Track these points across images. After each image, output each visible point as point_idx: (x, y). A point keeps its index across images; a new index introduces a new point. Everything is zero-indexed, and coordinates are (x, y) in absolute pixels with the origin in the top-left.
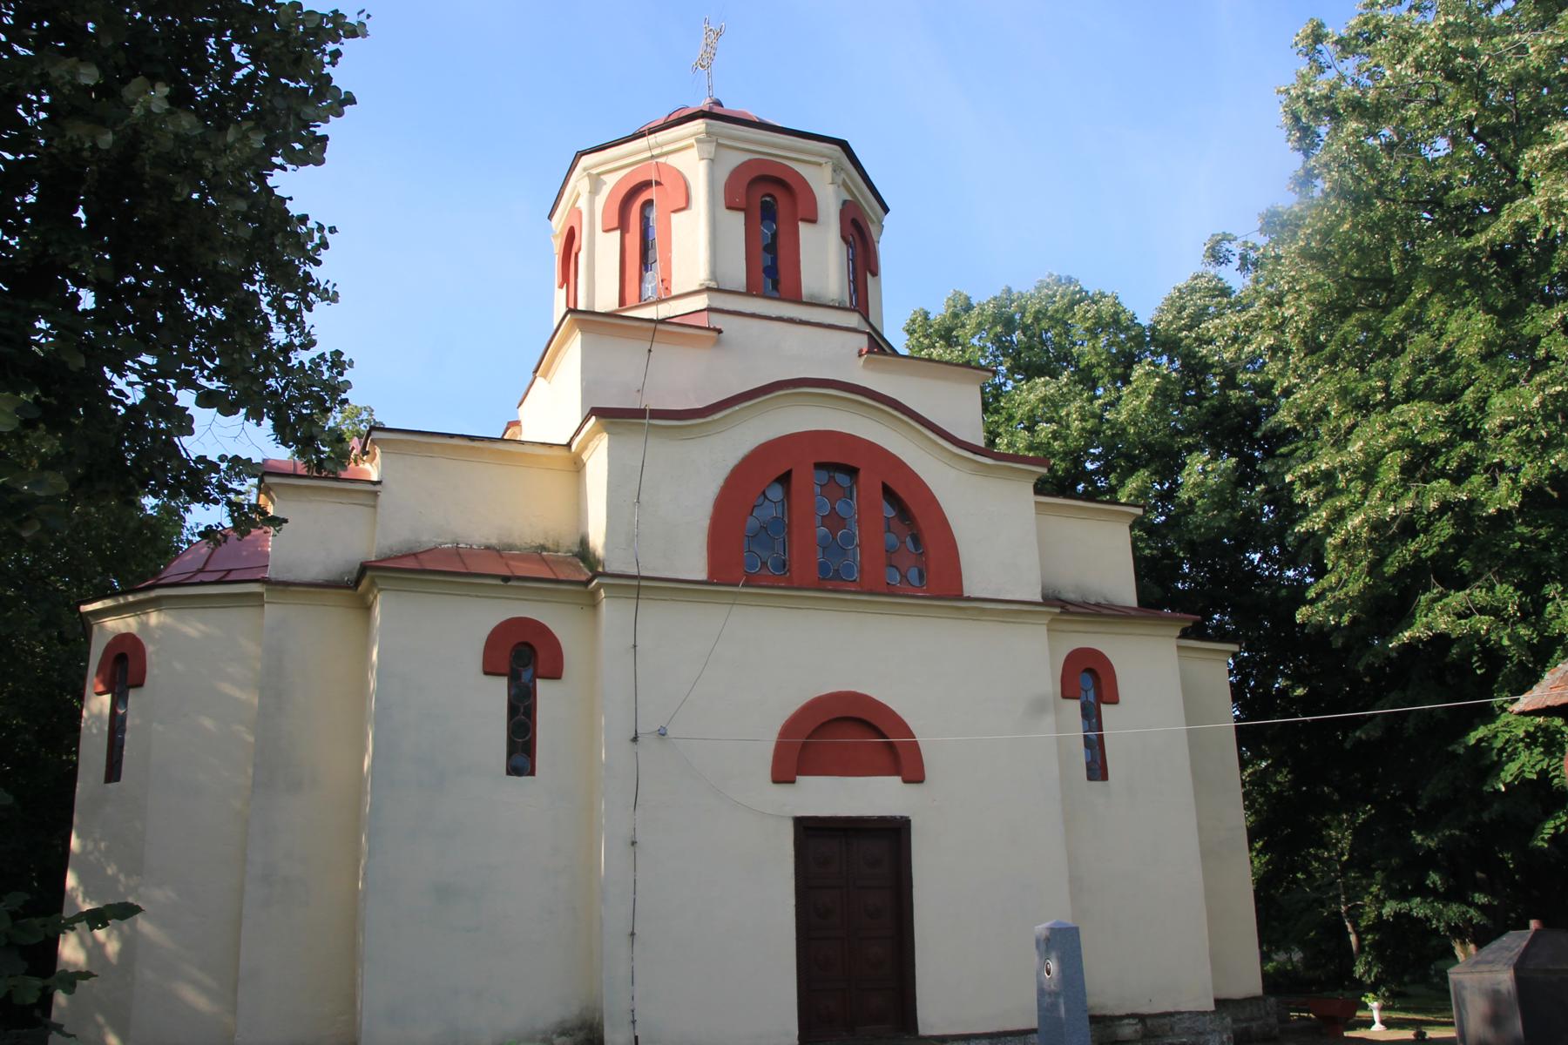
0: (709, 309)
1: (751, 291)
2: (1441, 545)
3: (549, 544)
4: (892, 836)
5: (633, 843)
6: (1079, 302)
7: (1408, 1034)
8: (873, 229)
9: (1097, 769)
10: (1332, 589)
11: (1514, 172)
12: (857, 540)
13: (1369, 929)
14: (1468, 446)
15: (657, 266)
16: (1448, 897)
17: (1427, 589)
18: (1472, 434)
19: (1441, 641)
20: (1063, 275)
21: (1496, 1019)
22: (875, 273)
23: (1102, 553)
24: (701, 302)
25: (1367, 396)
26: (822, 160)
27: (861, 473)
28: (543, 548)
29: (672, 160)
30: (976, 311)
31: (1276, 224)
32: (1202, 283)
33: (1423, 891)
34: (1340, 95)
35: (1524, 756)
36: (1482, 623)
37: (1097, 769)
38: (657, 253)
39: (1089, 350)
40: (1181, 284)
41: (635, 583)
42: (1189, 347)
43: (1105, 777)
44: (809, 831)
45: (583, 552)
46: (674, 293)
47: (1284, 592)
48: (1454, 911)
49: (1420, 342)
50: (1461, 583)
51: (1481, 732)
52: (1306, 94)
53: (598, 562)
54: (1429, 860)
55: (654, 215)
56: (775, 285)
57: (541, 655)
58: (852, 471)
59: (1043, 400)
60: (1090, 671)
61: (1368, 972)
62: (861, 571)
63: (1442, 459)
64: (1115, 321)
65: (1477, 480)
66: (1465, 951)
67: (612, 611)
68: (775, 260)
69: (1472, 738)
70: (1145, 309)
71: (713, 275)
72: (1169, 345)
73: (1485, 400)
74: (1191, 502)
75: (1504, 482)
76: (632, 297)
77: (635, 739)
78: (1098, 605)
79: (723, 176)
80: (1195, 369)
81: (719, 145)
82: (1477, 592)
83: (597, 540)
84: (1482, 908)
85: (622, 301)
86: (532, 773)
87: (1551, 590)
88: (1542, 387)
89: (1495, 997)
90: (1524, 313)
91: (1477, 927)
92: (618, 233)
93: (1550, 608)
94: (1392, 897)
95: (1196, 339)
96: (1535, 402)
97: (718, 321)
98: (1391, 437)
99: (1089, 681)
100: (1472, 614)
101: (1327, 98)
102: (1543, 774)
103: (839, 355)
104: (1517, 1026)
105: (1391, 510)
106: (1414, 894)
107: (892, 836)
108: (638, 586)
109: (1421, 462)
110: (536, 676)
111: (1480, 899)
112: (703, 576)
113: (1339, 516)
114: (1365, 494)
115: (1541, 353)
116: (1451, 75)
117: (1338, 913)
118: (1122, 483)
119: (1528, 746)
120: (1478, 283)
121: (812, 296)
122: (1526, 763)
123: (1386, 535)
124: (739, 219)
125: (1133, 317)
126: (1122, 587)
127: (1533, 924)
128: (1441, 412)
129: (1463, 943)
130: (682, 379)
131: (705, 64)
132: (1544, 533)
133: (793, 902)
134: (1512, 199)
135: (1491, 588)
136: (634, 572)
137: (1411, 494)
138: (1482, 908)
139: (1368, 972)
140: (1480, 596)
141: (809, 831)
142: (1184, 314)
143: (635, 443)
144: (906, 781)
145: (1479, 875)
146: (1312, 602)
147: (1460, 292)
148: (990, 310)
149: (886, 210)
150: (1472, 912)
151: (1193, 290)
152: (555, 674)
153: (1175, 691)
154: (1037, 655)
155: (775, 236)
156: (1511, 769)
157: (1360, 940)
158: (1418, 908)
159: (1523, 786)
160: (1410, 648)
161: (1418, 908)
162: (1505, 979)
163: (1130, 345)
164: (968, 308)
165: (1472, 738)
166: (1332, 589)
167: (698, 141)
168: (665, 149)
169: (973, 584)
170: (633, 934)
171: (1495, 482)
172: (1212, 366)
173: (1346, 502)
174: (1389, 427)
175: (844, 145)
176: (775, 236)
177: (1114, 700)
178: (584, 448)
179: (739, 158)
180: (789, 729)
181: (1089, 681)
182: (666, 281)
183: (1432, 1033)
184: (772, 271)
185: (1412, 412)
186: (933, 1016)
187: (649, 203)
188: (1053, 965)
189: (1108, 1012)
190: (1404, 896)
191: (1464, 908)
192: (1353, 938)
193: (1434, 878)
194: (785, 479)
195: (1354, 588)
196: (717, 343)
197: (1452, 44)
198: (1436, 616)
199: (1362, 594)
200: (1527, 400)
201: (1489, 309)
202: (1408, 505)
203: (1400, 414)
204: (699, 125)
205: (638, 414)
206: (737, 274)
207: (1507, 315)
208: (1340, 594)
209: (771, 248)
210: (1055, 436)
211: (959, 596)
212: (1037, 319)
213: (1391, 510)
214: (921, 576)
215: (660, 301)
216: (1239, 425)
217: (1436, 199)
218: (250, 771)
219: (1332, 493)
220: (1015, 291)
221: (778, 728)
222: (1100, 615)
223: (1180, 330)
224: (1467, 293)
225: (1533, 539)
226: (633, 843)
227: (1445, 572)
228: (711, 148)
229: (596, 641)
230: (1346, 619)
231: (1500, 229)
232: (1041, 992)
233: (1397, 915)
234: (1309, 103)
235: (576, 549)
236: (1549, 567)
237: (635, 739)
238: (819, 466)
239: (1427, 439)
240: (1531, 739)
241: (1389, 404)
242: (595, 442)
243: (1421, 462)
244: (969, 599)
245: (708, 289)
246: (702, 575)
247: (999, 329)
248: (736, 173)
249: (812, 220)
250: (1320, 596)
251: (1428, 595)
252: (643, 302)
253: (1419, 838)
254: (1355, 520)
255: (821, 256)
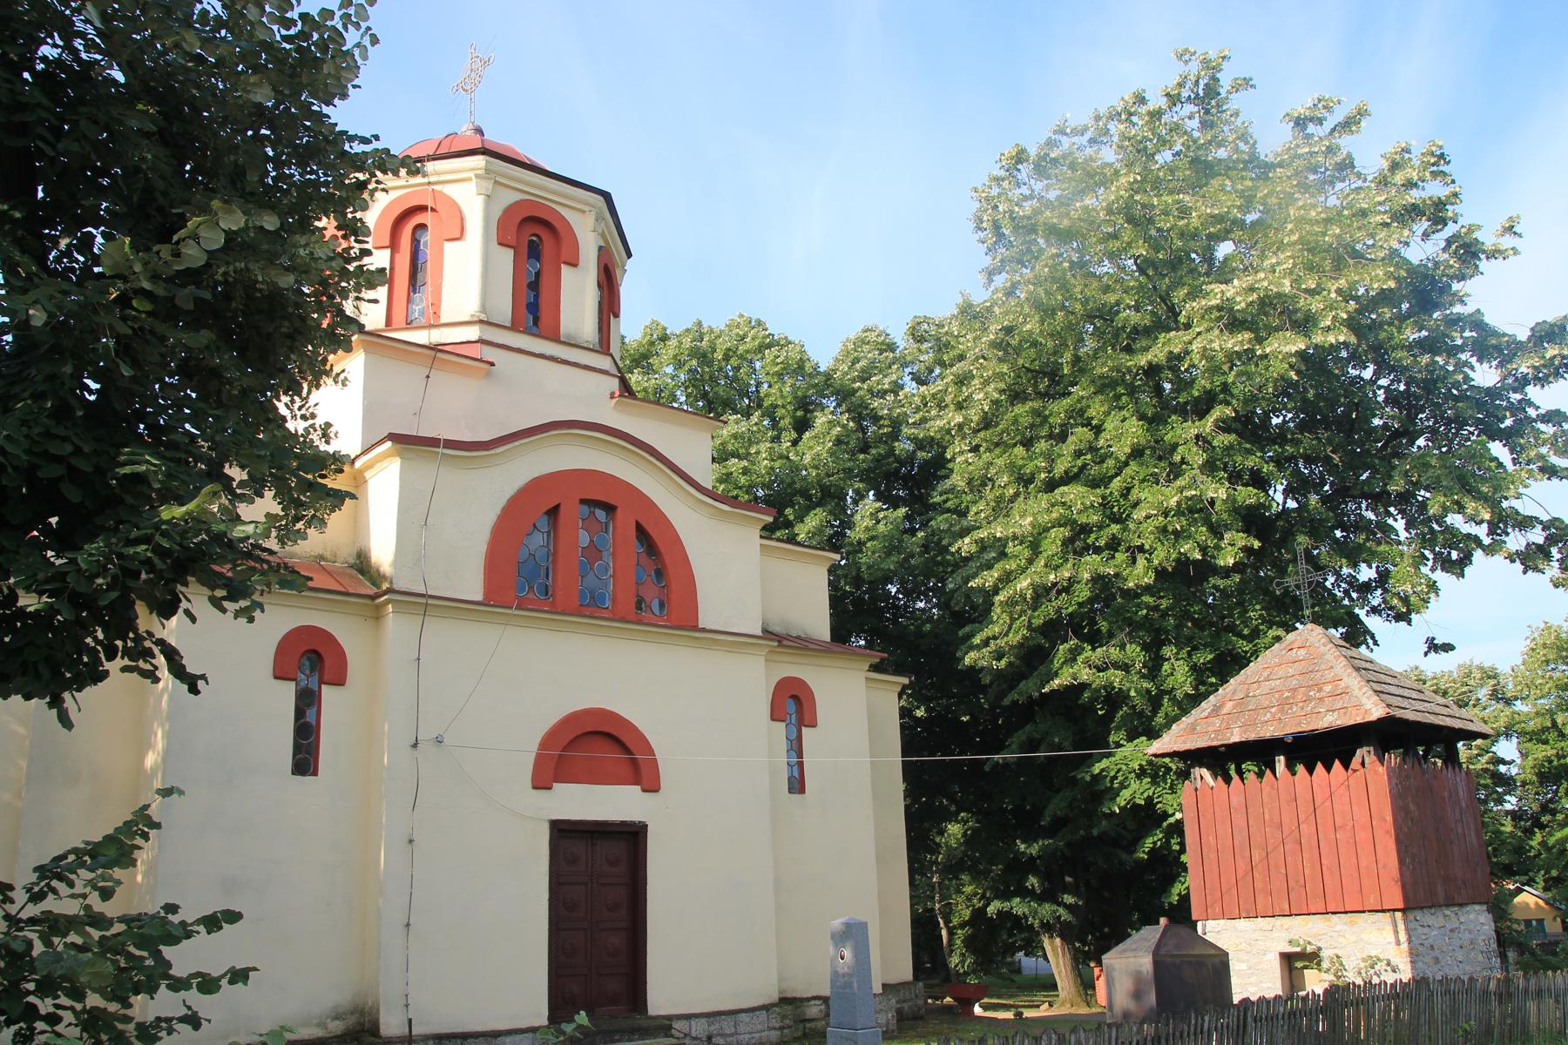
0: (481, 341)
1: (515, 327)
2: (1080, 605)
3: (328, 555)
4: (632, 837)
5: (411, 841)
6: (769, 346)
7: (1009, 1015)
8: (618, 272)
9: (797, 785)
10: (995, 638)
11: (1176, 315)
12: (611, 572)
13: (962, 925)
14: (1115, 528)
15: (429, 288)
16: (1042, 898)
17: (1065, 641)
18: (1116, 519)
19: (1079, 688)
20: (754, 318)
21: (1137, 995)
22: (617, 316)
23: (804, 591)
24: (473, 333)
25: (1033, 474)
26: (586, 208)
27: (619, 511)
28: (322, 557)
29: (448, 190)
30: (673, 343)
31: (970, 314)
32: (872, 336)
33: (1025, 893)
34: (1041, 219)
35: (1134, 785)
36: (1116, 677)
37: (797, 785)
38: (428, 275)
39: (778, 393)
40: (852, 336)
41: (423, 600)
42: (861, 398)
43: (802, 790)
44: (564, 833)
45: (362, 565)
46: (442, 321)
47: (928, 627)
48: (1046, 910)
49: (1080, 435)
50: (1095, 639)
51: (1104, 763)
52: (1012, 212)
53: (384, 577)
54: (1030, 865)
55: (426, 238)
56: (536, 321)
57: (328, 663)
58: (610, 509)
59: (735, 436)
60: (795, 697)
61: (963, 962)
62: (614, 601)
63: (1093, 536)
64: (799, 367)
65: (1121, 557)
66: (1052, 944)
67: (395, 623)
68: (537, 297)
69: (1097, 769)
70: (824, 355)
71: (483, 309)
72: (844, 395)
73: (1129, 489)
74: (861, 543)
75: (1141, 561)
76: (399, 318)
77: (415, 745)
78: (798, 637)
79: (497, 212)
80: (861, 413)
81: (496, 182)
82: (1112, 650)
83: (383, 553)
84: (1068, 907)
85: (389, 322)
86: (315, 773)
87: (1168, 651)
88: (1181, 490)
89: (1138, 979)
90: (1166, 422)
91: (1066, 924)
92: (388, 252)
93: (1166, 666)
94: (997, 897)
95: (870, 391)
96: (1173, 502)
97: (489, 353)
98: (1054, 515)
99: (793, 704)
100: (1107, 668)
101: (1029, 218)
102: (1149, 799)
103: (590, 396)
104: (1152, 999)
105: (1052, 577)
106: (1015, 894)
107: (632, 837)
108: (424, 603)
109: (1078, 540)
110: (321, 682)
111: (1069, 899)
112: (479, 597)
113: (1007, 578)
114: (1030, 562)
115: (1177, 458)
116: (1131, 220)
117: (933, 910)
118: (800, 518)
119: (1138, 777)
120: (1132, 391)
121: (568, 336)
122: (1135, 791)
123: (1042, 593)
124: (509, 255)
125: (817, 366)
126: (819, 623)
127: (1163, 921)
128: (1094, 497)
129: (1051, 937)
130: (455, 408)
131: (467, 87)
132: (1164, 604)
133: (546, 896)
134: (1169, 330)
135: (1123, 647)
136: (422, 590)
137: (1069, 565)
138: (1068, 907)
139: (963, 962)
140: (1114, 653)
141: (564, 833)
142: (858, 366)
143: (429, 469)
144: (644, 790)
145: (1068, 879)
146: (978, 647)
147: (1118, 397)
148: (687, 342)
149: (629, 255)
150: (1061, 911)
151: (864, 342)
152: (340, 681)
153: (861, 712)
154: (755, 678)
155: (538, 274)
156: (1125, 794)
157: (951, 933)
158: (1018, 906)
159: (1133, 810)
160: (1053, 691)
161: (1018, 906)
162: (1145, 963)
163: (811, 393)
164: (664, 338)
165: (1097, 769)
166: (995, 638)
167: (477, 176)
168: (443, 178)
169: (708, 616)
170: (408, 925)
171: (1134, 561)
172: (882, 418)
173: (1014, 566)
174: (1053, 505)
175: (607, 196)
176: (538, 274)
177: (813, 725)
178: (369, 466)
179: (512, 197)
180: (547, 742)
181: (793, 704)
182: (436, 305)
183: (1028, 1013)
184: (534, 308)
185: (1074, 494)
186: (662, 997)
187: (422, 227)
188: (847, 953)
189: (798, 995)
190: (1005, 896)
191: (1055, 907)
192: (944, 933)
193: (1033, 881)
194: (553, 512)
195: (1014, 638)
196: (488, 374)
197: (1137, 197)
198: (1075, 669)
199: (1021, 645)
200: (1168, 498)
201: (1142, 417)
202: (1067, 575)
203: (1062, 495)
204: (479, 161)
205: (433, 442)
206: (504, 308)
207: (1154, 421)
208: (1001, 642)
209: (534, 286)
210: (745, 471)
211: (695, 628)
212: (727, 358)
213: (1052, 577)
214: (662, 605)
215: (431, 326)
216: (912, 478)
217: (1104, 315)
218: (24, 764)
219: (1003, 555)
220: (705, 325)
221: (538, 740)
222: (806, 648)
223: (854, 381)
224: (1124, 399)
225: (1156, 608)
226: (411, 841)
227: (1084, 627)
228: (490, 185)
229: (380, 652)
230: (1003, 663)
231: (1157, 353)
232: (835, 974)
233: (1000, 913)
234: (1013, 219)
235: (352, 561)
236: (1167, 632)
237: (415, 745)
238: (583, 501)
239: (1083, 520)
240: (1141, 773)
241: (1051, 486)
242: (385, 463)
243: (1078, 540)
244: (704, 630)
245: (481, 322)
246: (478, 596)
247: (694, 362)
248: (509, 211)
249: (574, 264)
250: (986, 643)
251: (1066, 646)
252: (409, 325)
253: (1023, 847)
254: (1023, 584)
255: (577, 295)
